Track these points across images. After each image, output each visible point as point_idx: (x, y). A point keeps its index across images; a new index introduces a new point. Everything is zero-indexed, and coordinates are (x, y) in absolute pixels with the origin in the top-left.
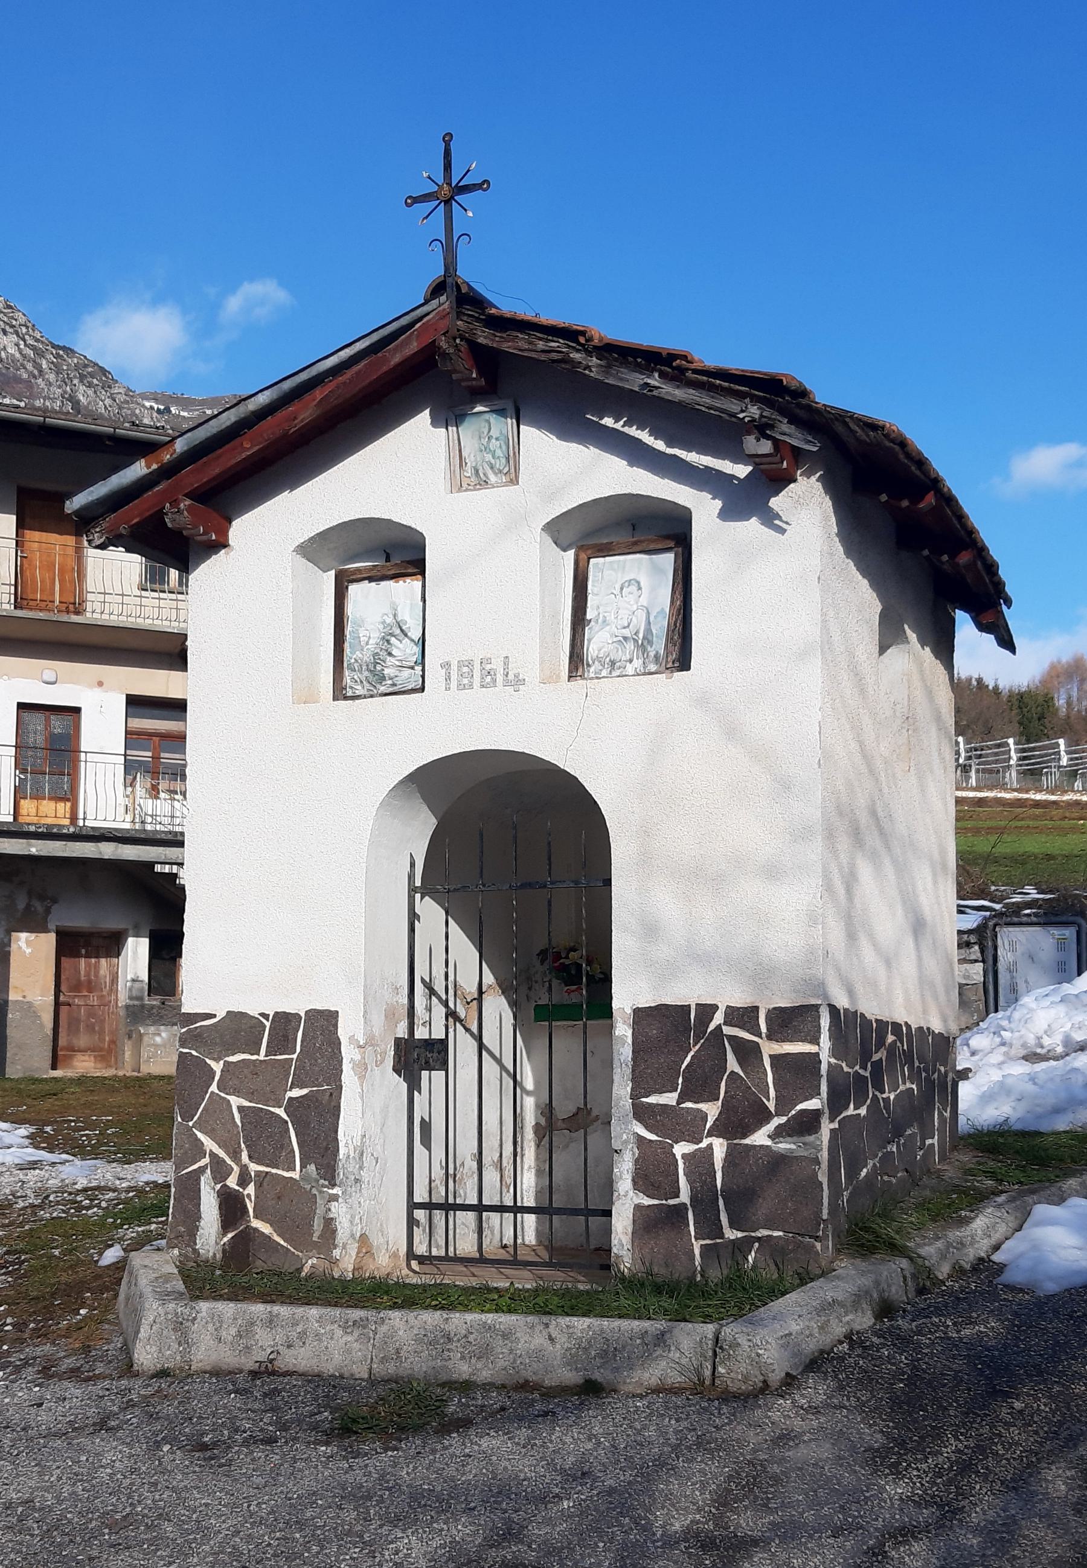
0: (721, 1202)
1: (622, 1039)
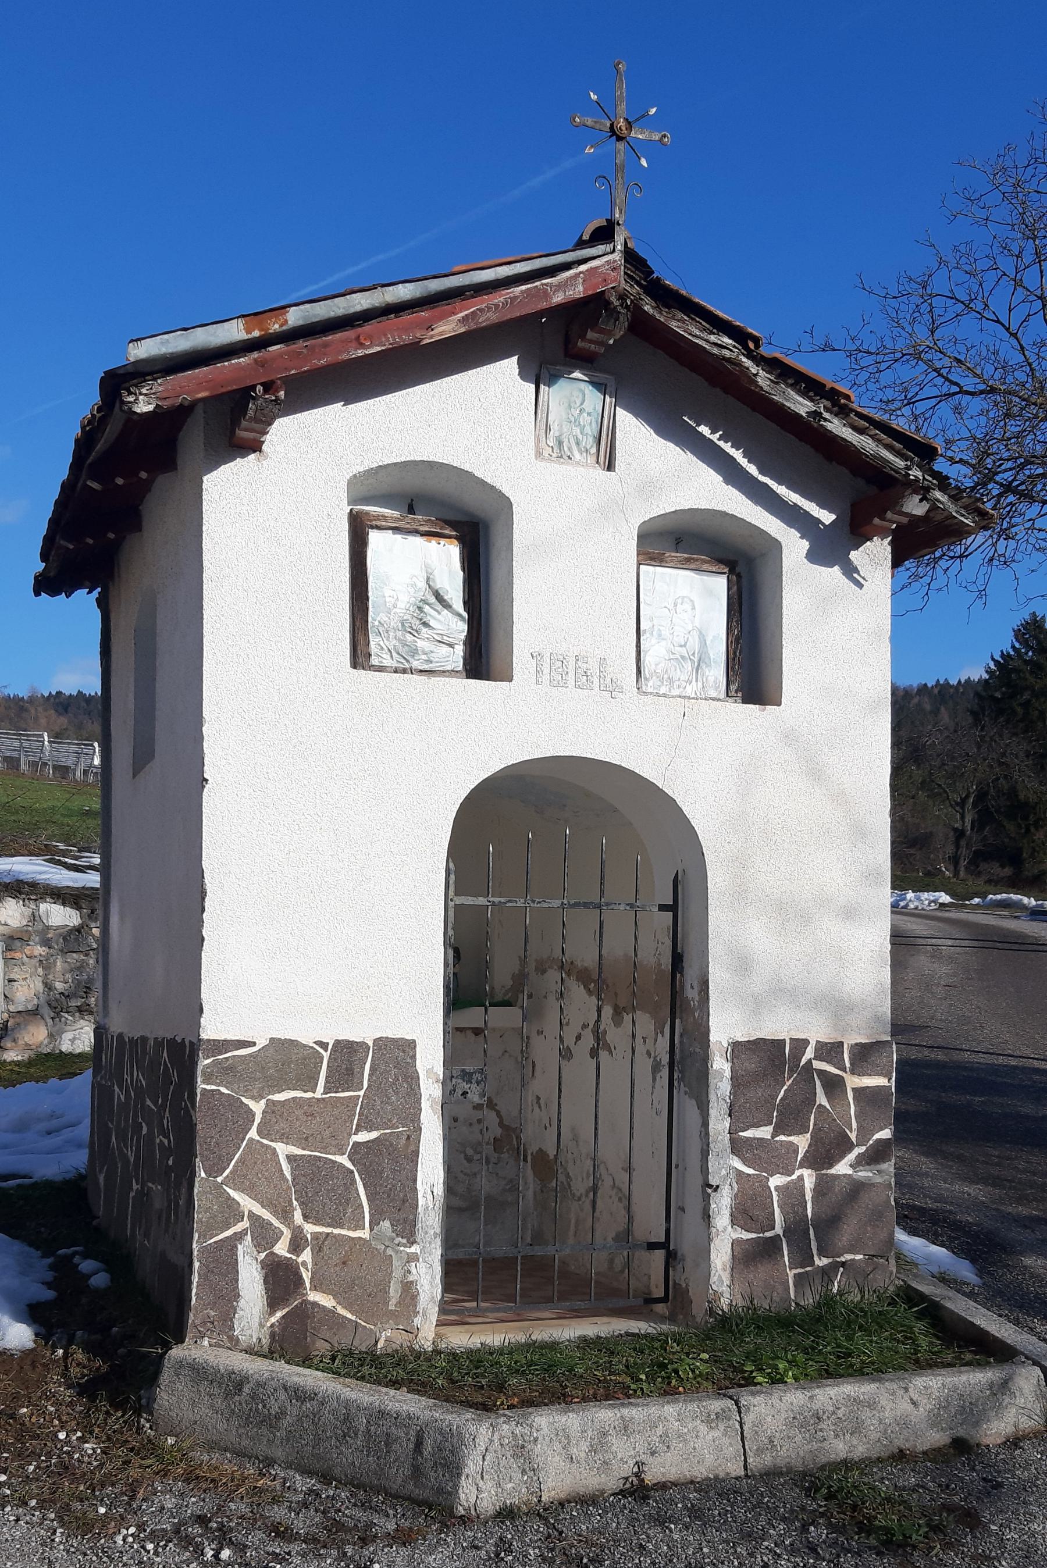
1: (720, 1073)
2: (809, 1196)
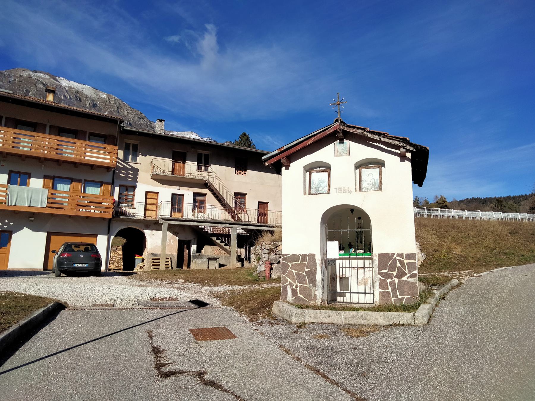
2: (396, 284)
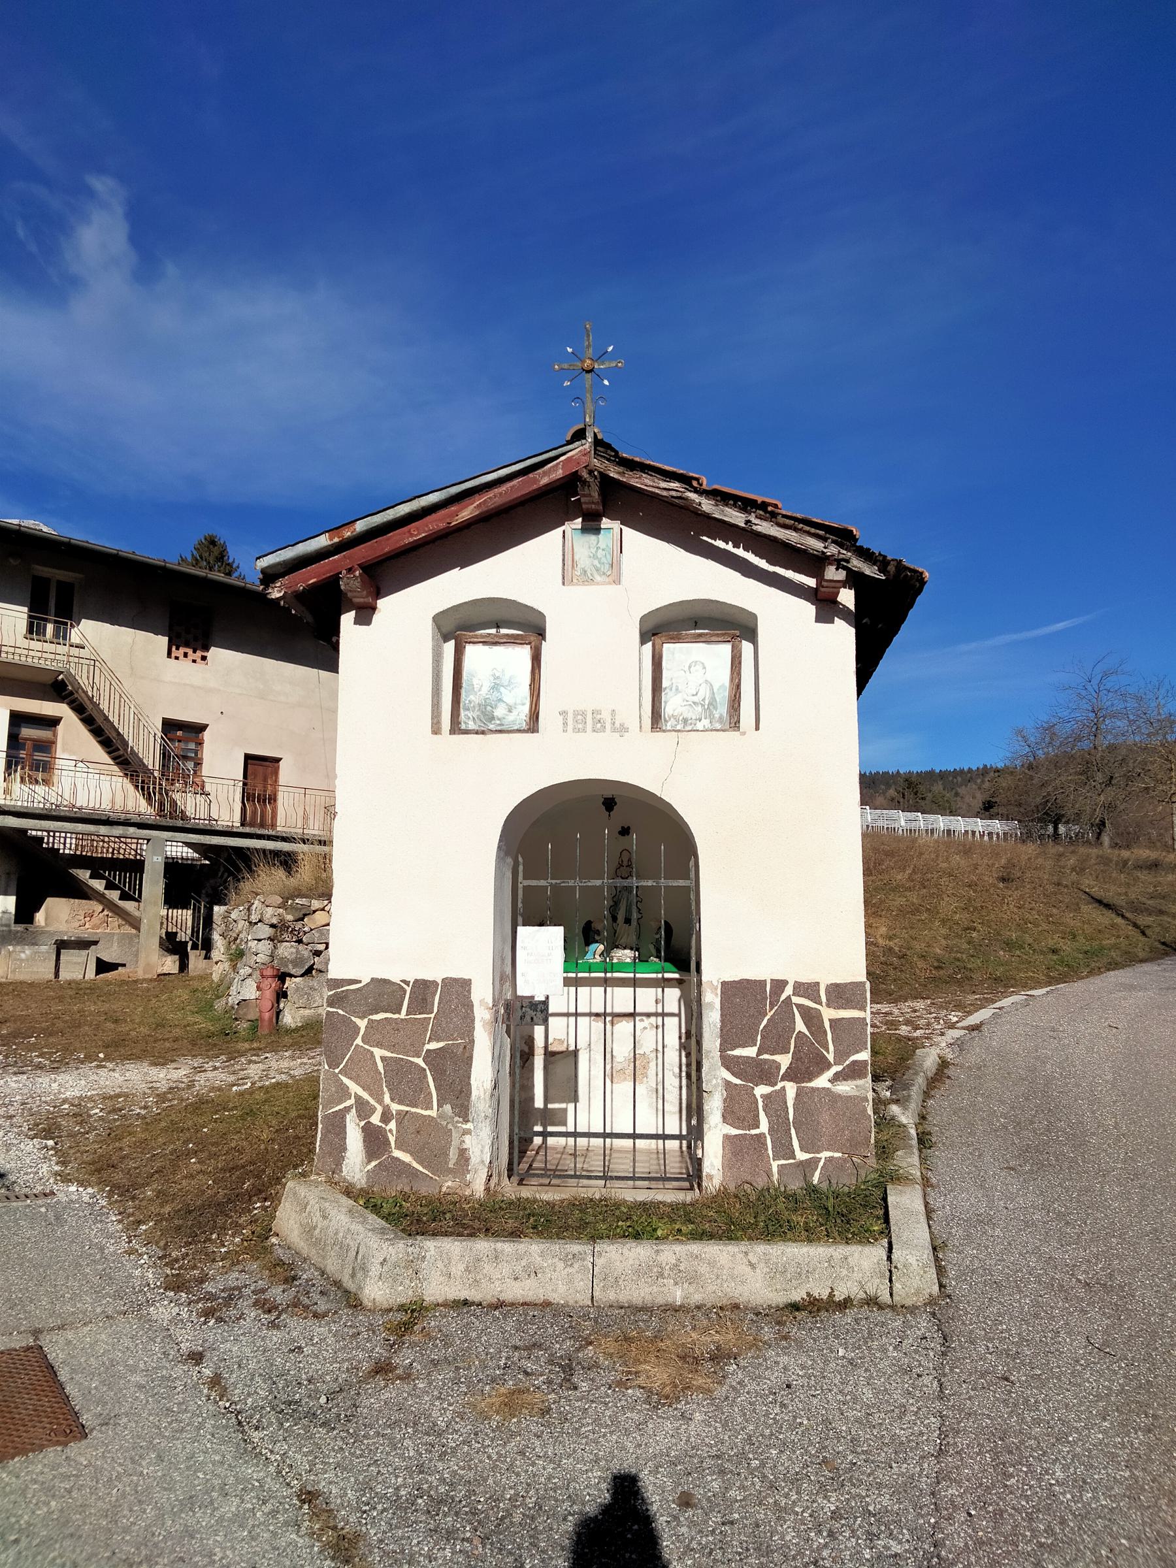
0: (793, 1131)
1: (711, 1005)
